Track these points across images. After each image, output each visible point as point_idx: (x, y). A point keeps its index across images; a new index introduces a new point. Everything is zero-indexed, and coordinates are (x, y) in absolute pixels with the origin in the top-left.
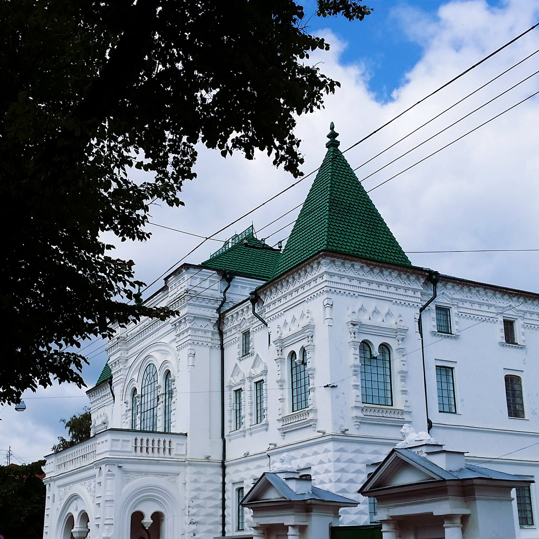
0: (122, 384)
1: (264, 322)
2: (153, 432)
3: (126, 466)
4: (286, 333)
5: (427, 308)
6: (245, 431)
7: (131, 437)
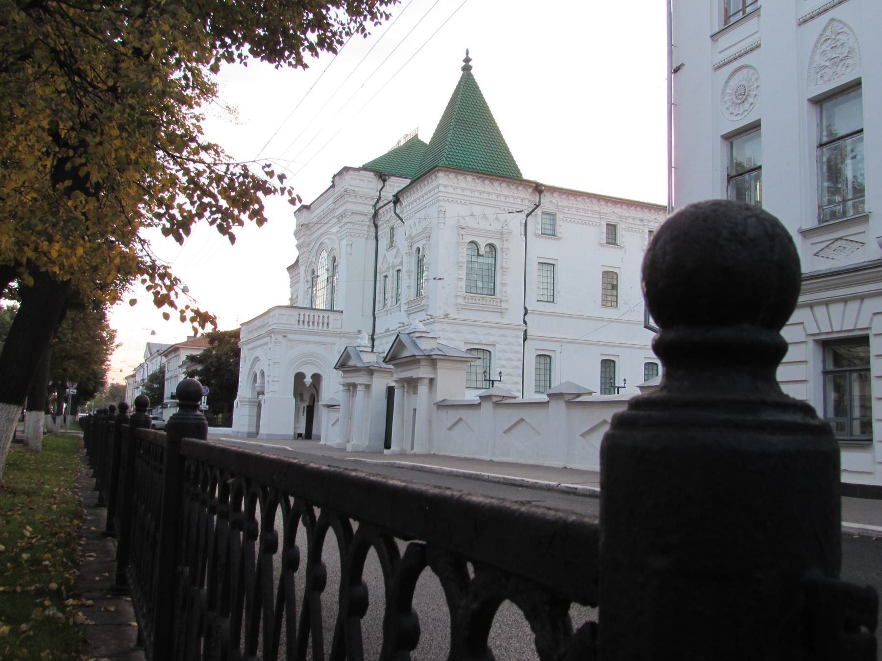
0: (305, 265)
1: (402, 220)
2: (311, 309)
3: (290, 336)
4: (415, 232)
5: (533, 213)
6: (387, 311)
7: (295, 313)
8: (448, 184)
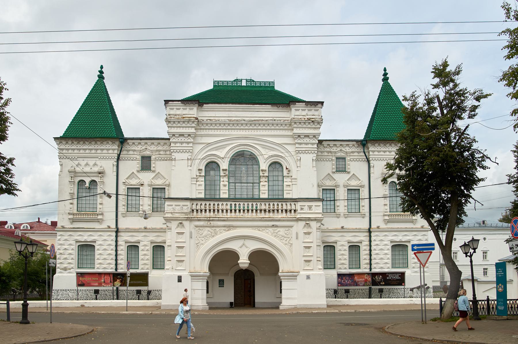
8: (374, 150)
